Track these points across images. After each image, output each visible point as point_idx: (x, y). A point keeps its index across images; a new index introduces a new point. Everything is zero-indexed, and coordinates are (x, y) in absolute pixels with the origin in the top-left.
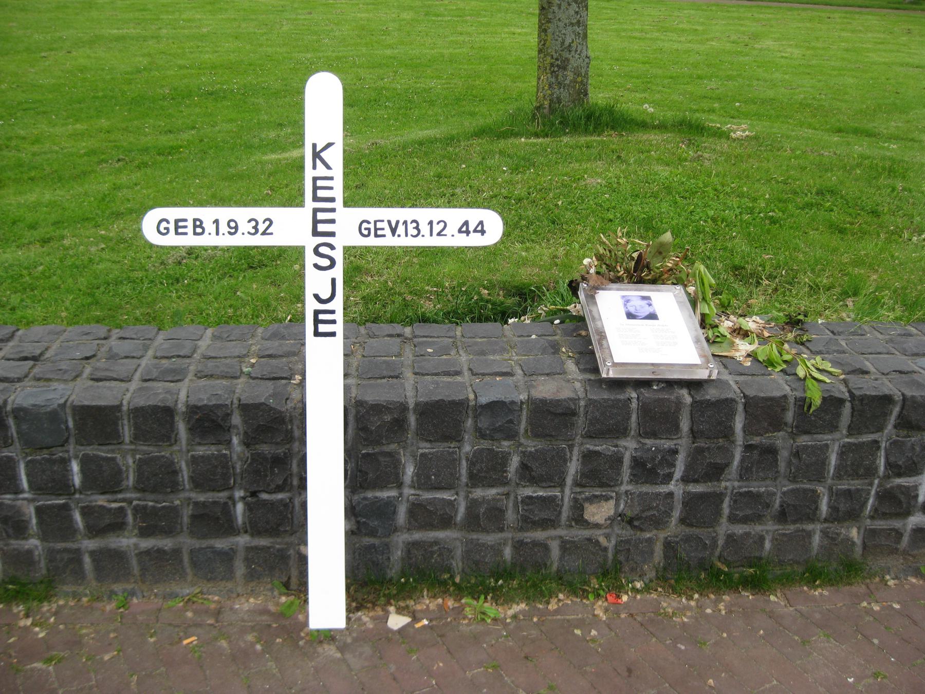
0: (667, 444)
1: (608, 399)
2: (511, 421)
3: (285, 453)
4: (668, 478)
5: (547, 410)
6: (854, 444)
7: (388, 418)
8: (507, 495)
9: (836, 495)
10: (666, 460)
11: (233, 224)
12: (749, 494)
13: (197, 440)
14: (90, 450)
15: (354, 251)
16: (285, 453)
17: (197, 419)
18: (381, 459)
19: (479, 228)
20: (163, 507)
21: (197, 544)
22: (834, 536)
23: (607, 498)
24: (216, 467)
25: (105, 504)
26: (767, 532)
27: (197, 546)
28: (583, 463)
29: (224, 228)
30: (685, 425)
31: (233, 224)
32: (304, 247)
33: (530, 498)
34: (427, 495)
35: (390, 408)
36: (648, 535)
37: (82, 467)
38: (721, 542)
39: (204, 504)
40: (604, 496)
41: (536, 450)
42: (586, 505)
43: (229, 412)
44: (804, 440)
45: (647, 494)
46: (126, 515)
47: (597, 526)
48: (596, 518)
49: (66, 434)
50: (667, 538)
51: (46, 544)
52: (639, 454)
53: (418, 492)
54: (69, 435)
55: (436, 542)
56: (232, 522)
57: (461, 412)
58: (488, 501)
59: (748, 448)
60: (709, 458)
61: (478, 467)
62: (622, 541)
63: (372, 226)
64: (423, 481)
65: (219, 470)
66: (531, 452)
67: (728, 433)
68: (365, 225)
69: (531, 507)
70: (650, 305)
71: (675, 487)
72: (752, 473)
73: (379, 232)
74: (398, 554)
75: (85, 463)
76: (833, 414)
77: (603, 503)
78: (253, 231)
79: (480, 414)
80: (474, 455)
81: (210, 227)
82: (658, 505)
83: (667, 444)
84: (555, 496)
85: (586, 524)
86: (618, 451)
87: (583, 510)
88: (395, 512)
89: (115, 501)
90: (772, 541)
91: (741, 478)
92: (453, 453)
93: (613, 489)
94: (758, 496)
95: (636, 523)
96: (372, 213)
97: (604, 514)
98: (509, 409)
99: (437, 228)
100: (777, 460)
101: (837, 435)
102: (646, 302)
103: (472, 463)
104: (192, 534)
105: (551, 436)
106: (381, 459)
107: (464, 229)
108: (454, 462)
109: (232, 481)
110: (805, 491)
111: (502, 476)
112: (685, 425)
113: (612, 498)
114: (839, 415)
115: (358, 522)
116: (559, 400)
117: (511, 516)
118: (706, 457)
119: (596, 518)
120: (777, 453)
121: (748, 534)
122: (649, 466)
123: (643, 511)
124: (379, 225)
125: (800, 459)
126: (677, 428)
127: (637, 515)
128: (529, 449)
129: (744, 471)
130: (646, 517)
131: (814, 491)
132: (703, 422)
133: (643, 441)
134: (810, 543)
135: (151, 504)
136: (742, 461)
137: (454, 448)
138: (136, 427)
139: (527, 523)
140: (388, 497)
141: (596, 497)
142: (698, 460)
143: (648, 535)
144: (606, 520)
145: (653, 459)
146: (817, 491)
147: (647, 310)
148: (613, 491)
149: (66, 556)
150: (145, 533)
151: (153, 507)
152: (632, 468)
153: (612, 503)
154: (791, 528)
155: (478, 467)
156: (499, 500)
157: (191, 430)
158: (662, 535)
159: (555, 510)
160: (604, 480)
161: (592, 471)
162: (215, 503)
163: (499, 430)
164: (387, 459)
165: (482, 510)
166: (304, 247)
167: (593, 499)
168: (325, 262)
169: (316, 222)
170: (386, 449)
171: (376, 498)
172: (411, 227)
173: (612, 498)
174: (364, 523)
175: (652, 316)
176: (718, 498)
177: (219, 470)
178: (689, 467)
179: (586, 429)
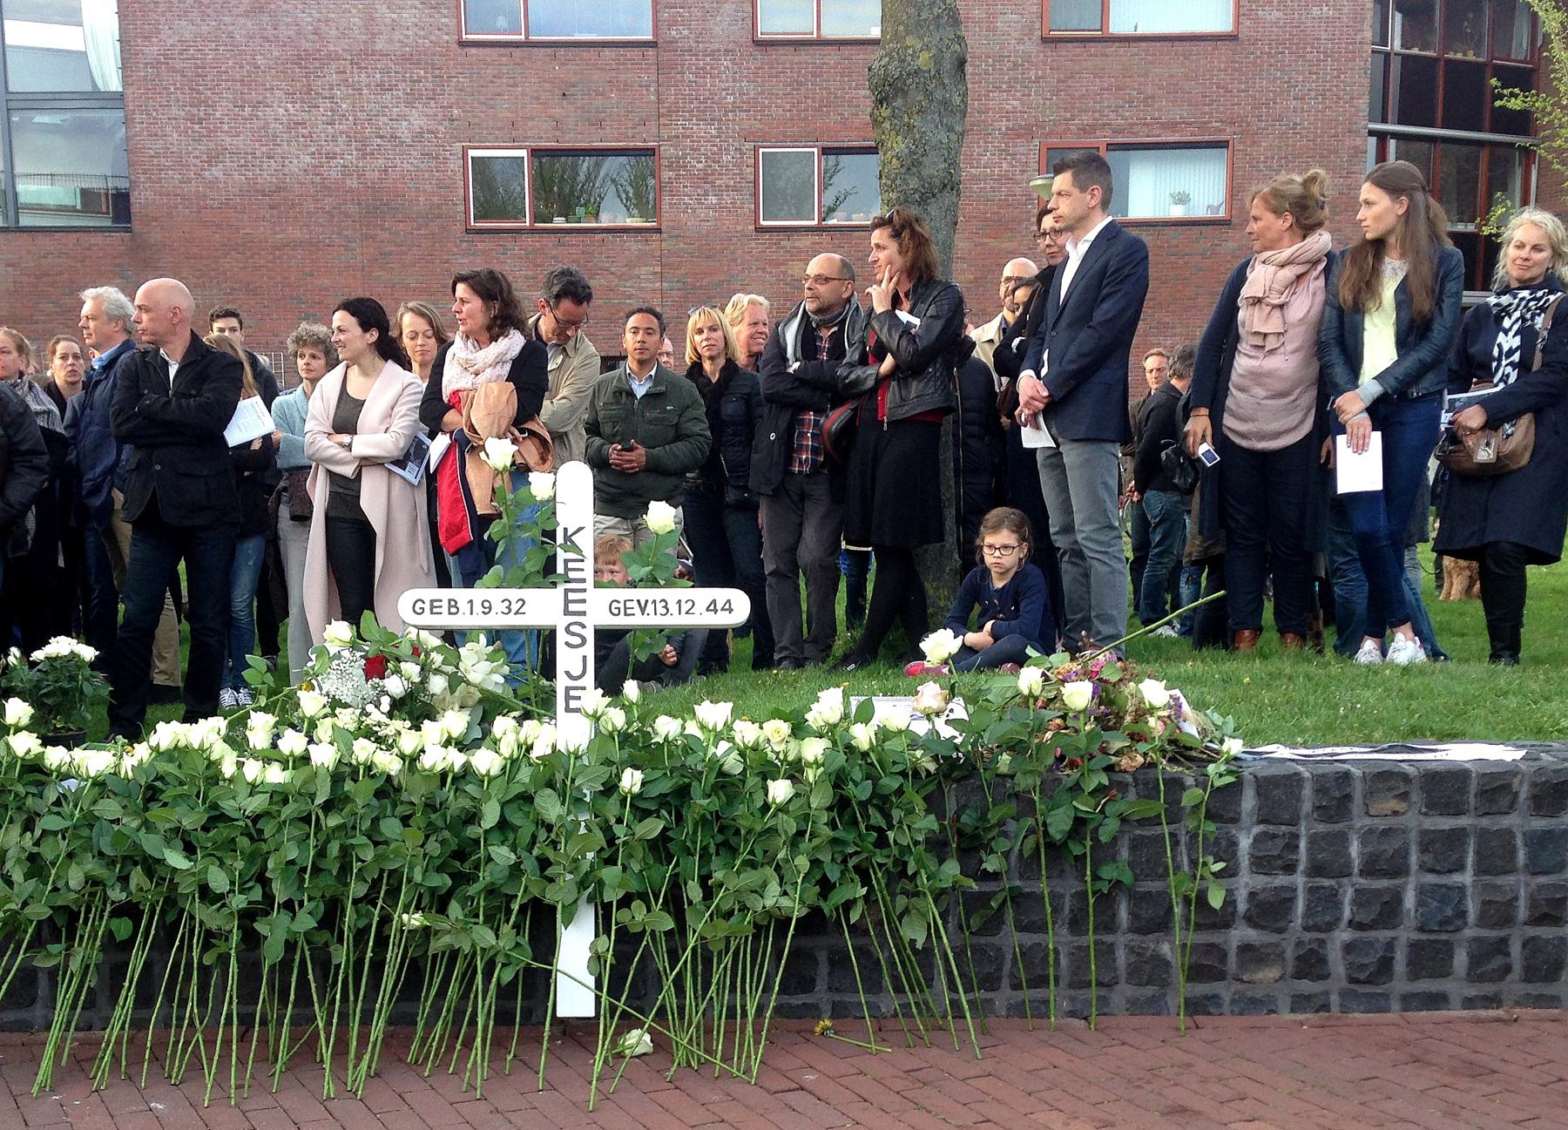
11: (486, 604)
99: (685, 607)
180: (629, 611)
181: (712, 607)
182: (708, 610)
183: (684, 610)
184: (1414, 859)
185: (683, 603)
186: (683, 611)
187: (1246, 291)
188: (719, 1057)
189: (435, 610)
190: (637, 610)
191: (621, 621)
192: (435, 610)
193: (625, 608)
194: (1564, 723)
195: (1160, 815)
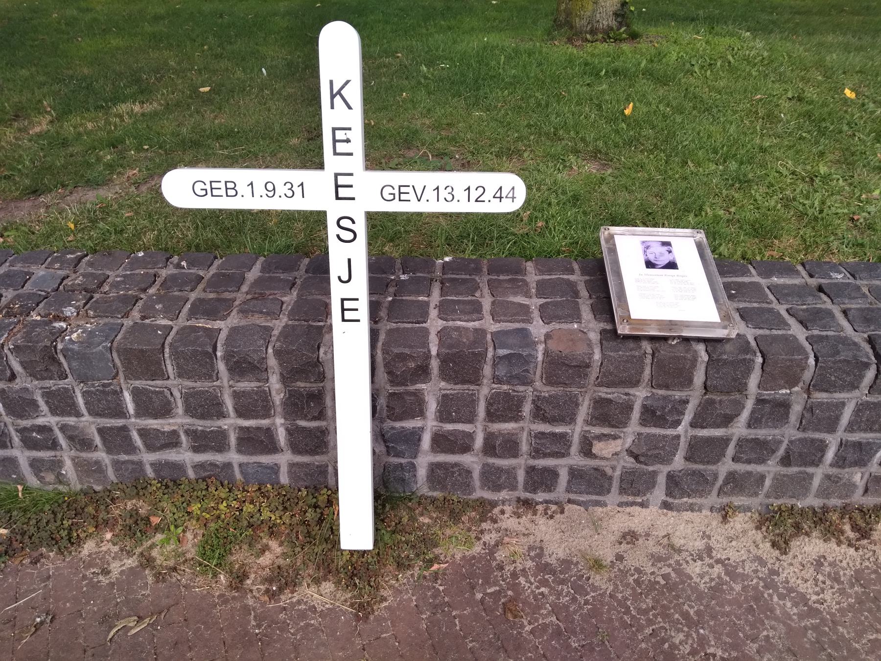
0: (677, 395)
2: (527, 371)
3: (319, 391)
4: (678, 423)
5: (562, 362)
6: (873, 403)
7: (412, 365)
8: (523, 428)
9: (846, 446)
10: (676, 408)
11: (270, 187)
12: (756, 441)
13: (237, 378)
14: (138, 383)
15: (509, 216)
16: (319, 391)
17: (235, 362)
18: (407, 398)
19: (511, 195)
21: (244, 459)
22: (836, 479)
23: (615, 437)
24: (257, 400)
26: (769, 472)
27: (245, 461)
28: (595, 408)
30: (699, 378)
31: (270, 187)
32: (325, 213)
33: (543, 433)
34: (449, 427)
35: (413, 357)
36: (651, 468)
37: (133, 397)
39: (248, 428)
40: (612, 435)
41: (549, 396)
42: (595, 442)
43: (264, 356)
44: (821, 396)
45: (654, 435)
46: (179, 436)
47: (603, 458)
48: (603, 452)
49: (115, 371)
50: (670, 472)
51: (111, 457)
52: (649, 402)
53: (440, 424)
54: (118, 372)
55: (456, 465)
56: (275, 444)
58: (503, 435)
59: (760, 401)
60: (720, 410)
61: (495, 407)
62: (626, 472)
64: (444, 415)
65: (260, 403)
66: (545, 397)
67: (742, 388)
69: (543, 441)
70: (670, 252)
71: (680, 429)
73: (403, 197)
74: (422, 473)
75: (137, 394)
76: (855, 376)
78: (290, 193)
79: (498, 364)
80: (491, 398)
82: (664, 446)
83: (677, 395)
84: (566, 433)
86: (629, 399)
88: (419, 440)
90: (773, 479)
91: (749, 426)
92: (472, 394)
93: (621, 429)
94: (764, 443)
95: (642, 459)
96: (396, 178)
98: (526, 361)
99: (474, 195)
100: (789, 413)
101: (856, 393)
102: (666, 248)
103: (489, 404)
104: (239, 451)
105: (565, 384)
106: (407, 398)
107: (498, 195)
108: (472, 402)
109: (273, 412)
110: (813, 441)
111: (517, 415)
112: (699, 378)
114: (861, 377)
115: (387, 447)
117: (524, 447)
118: (717, 408)
119: (603, 452)
120: (790, 407)
122: (658, 413)
123: (649, 450)
126: (690, 381)
128: (543, 394)
129: (753, 421)
130: (652, 455)
133: (654, 391)
134: (811, 483)
138: (179, 366)
139: (537, 453)
140: (414, 428)
141: (605, 435)
143: (651, 468)
144: (613, 455)
145: (663, 408)
146: (825, 441)
147: (665, 259)
149: (130, 467)
150: (196, 450)
152: (642, 414)
154: (794, 470)
155: (495, 407)
157: (231, 370)
158: (665, 469)
159: (565, 444)
160: (614, 423)
161: (602, 415)
162: (258, 429)
163: (517, 377)
164: (412, 398)
165: (498, 443)
166: (325, 213)
167: (601, 437)
169: (337, 186)
170: (412, 388)
171: (403, 428)
174: (393, 447)
175: (672, 265)
176: (725, 441)
177: (260, 403)
178: (696, 415)
179: (599, 380)
180: (403, 197)
181: (231, 189)
182: (494, 197)
183: (473, 197)
184: (487, 370)
185: (441, 189)
186: (473, 198)
187: (108, 280)
188: (741, 468)
189: (342, 192)
190: (412, 196)
191: (396, 207)
192: (342, 192)
193: (400, 193)
194: (3, 184)
195: (781, 442)
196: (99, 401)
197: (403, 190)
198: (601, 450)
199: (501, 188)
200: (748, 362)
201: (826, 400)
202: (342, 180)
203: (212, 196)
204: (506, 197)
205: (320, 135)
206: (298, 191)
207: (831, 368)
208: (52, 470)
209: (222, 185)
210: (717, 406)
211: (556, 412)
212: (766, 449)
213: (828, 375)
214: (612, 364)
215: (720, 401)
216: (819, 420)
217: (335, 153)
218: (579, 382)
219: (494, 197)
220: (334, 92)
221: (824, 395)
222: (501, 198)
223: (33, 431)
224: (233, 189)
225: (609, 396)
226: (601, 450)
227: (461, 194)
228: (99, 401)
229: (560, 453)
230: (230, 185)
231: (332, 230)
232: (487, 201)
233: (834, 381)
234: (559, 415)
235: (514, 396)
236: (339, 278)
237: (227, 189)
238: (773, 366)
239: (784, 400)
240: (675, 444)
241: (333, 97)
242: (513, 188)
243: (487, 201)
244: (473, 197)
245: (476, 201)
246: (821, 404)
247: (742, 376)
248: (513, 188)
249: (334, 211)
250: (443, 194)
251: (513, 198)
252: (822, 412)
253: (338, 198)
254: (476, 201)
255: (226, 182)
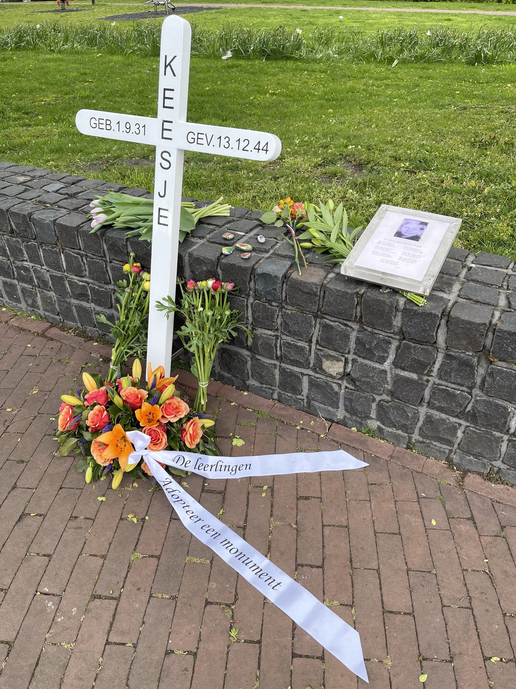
1: (340, 291)
19: (265, 148)
20: (102, 291)
23: (338, 360)
25: (77, 282)
29: (123, 128)
38: (422, 419)
47: (331, 376)
57: (246, 275)
60: (414, 355)
63: (97, 122)
66: (288, 313)
68: (93, 121)
72: (451, 377)
77: (335, 362)
81: (114, 126)
82: (373, 376)
84: (305, 347)
85: (323, 371)
86: (346, 330)
87: (322, 363)
89: (82, 281)
97: (336, 369)
99: (243, 145)
107: (257, 147)
113: (341, 360)
116: (305, 283)
121: (444, 421)
122: (367, 346)
124: (200, 136)
125: (494, 380)
127: (358, 378)
129: (443, 374)
131: (506, 409)
132: (411, 326)
135: (97, 287)
136: (442, 365)
137: (244, 298)
142: (406, 354)
145: (371, 343)
146: (508, 410)
148: (343, 356)
151: (97, 289)
153: (342, 364)
156: (270, 339)
160: (336, 347)
168: (165, 155)
169: (163, 129)
172: (224, 142)
173: (341, 360)
182: (254, 149)
185: (222, 138)
186: (241, 147)
189: (166, 134)
190: (204, 142)
192: (166, 134)
196: (49, 256)
197: (200, 136)
198: (329, 368)
199: (259, 142)
200: (434, 318)
201: (505, 369)
202: (167, 126)
203: (197, 143)
204: (262, 150)
205: (157, 92)
206: (142, 129)
207: (507, 339)
208: (31, 297)
209: (104, 122)
210: (412, 351)
211: (296, 328)
212: (455, 402)
213: (505, 345)
214: (332, 296)
215: (414, 347)
216: (500, 387)
217: (164, 107)
218: (311, 307)
219: (254, 149)
220: (167, 64)
221: (504, 364)
222: (259, 149)
223: (22, 269)
224: (109, 125)
225: (332, 323)
226: (329, 368)
227: (234, 144)
228: (49, 256)
229: (300, 362)
230: (108, 122)
231: (158, 160)
232: (250, 151)
233: (511, 352)
234: (298, 331)
235: (269, 308)
236: (159, 193)
237: (106, 124)
238: (455, 325)
239: (468, 359)
240: (383, 378)
241: (166, 67)
242: (267, 144)
243: (250, 151)
244: (241, 147)
245: (243, 150)
246: (500, 372)
247: (430, 328)
248: (267, 144)
249: (161, 146)
250: (224, 142)
251: (267, 150)
252: (502, 380)
253: (163, 138)
254: (243, 150)
255: (106, 120)
